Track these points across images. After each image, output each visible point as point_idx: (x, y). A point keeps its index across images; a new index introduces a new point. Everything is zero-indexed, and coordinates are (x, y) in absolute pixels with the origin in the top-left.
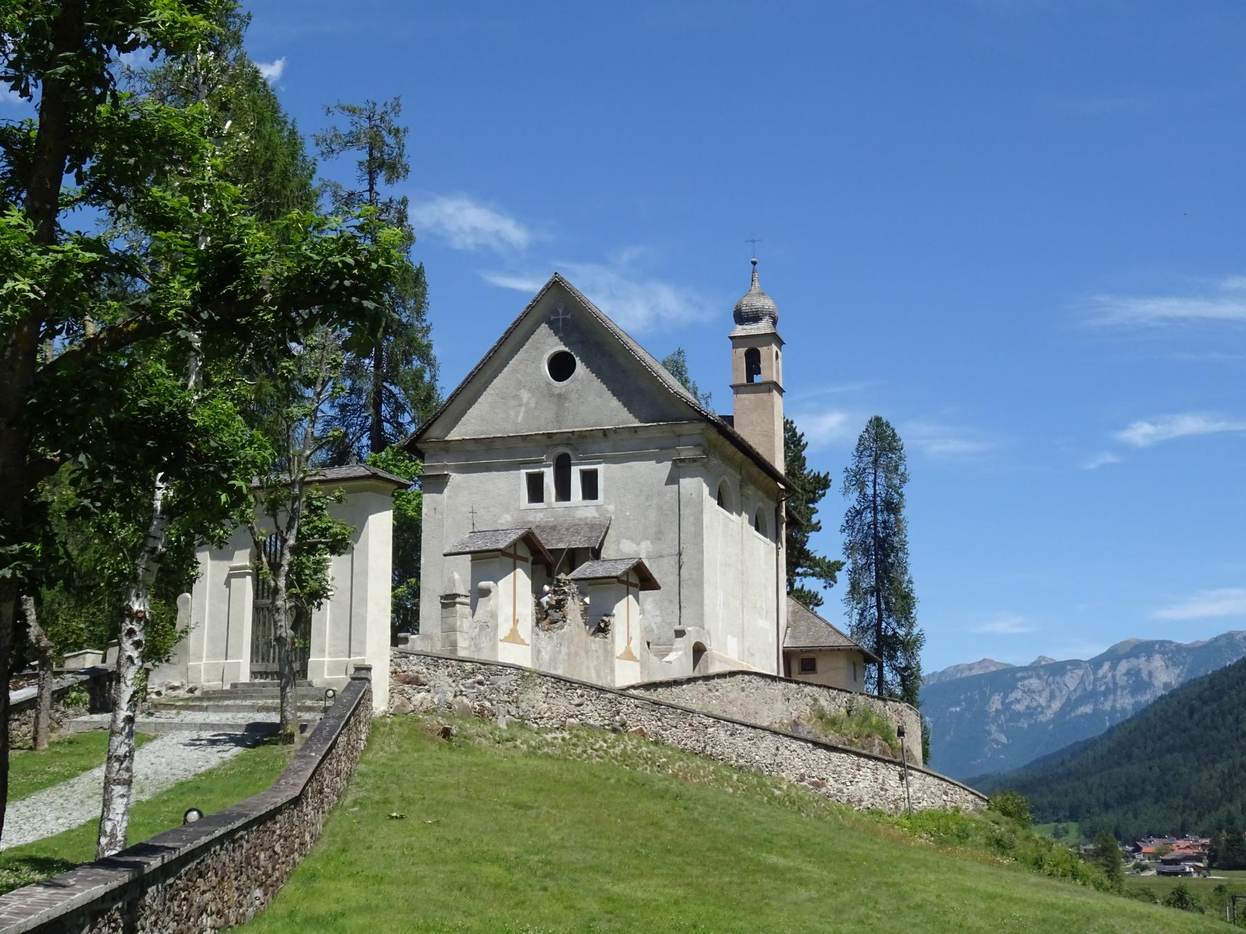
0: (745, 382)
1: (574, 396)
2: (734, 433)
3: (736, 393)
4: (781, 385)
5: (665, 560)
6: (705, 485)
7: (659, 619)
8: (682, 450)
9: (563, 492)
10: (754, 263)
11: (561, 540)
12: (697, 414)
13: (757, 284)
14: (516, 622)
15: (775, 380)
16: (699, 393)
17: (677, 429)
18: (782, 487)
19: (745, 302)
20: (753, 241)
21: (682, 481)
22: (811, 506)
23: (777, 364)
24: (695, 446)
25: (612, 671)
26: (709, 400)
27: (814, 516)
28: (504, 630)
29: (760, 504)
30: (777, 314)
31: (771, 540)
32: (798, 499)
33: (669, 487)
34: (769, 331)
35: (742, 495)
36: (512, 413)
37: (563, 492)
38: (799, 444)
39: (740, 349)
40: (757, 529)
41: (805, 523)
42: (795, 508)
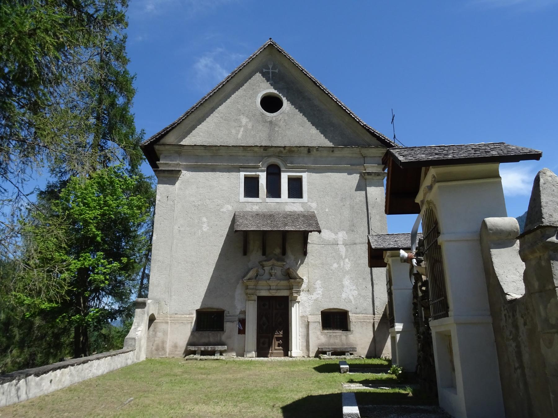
1: (281, 123)
5: (358, 247)
7: (356, 293)
36: (234, 131)
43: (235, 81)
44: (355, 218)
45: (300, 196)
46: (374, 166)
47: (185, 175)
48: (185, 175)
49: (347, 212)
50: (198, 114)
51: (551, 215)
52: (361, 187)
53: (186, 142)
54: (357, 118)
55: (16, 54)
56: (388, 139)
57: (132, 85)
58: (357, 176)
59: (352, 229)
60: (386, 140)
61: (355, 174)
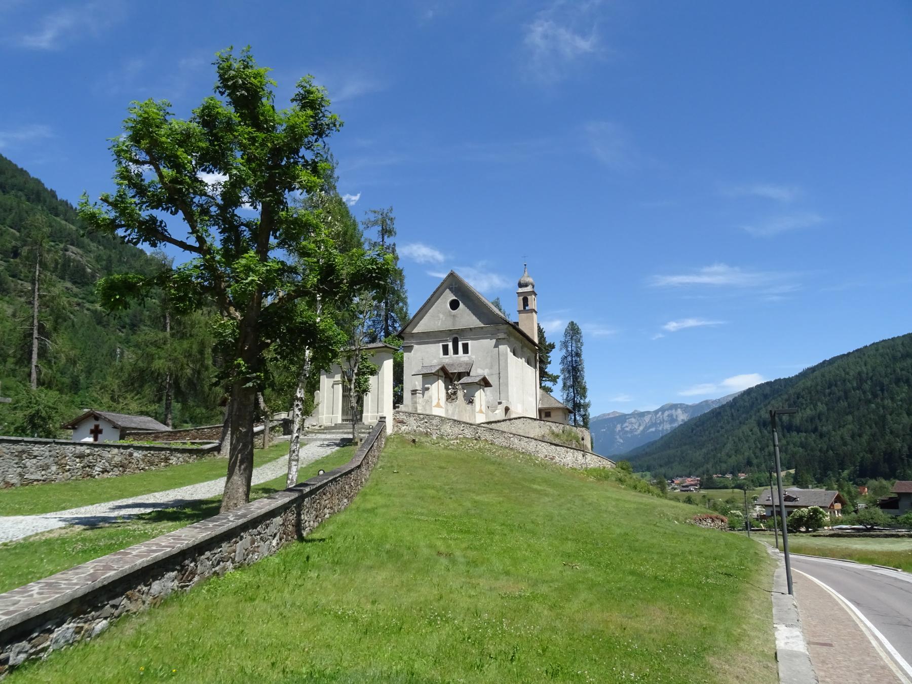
9: (456, 352)
11: (455, 369)
14: (439, 399)
25: (475, 417)
28: (434, 403)
37: (456, 352)
43: (437, 295)
45: (468, 353)
47: (416, 347)
48: (416, 347)
50: (419, 316)
51: (99, 323)
52: (496, 346)
53: (415, 331)
55: (378, 315)
57: (229, 99)
58: (495, 340)
59: (491, 368)
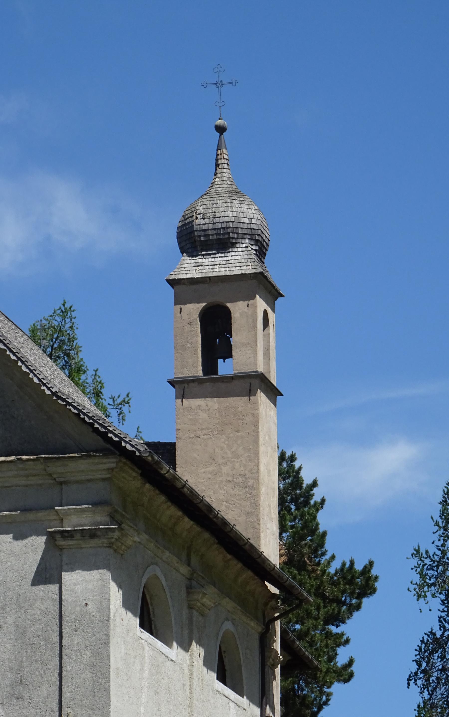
0: (202, 376)
2: (176, 478)
3: (182, 396)
4: (274, 381)
6: (113, 587)
8: (67, 513)
10: (221, 130)
12: (101, 443)
13: (225, 172)
15: (261, 369)
16: (106, 393)
17: (54, 468)
18: (274, 590)
19: (200, 209)
20: (219, 85)
21: (67, 577)
22: (333, 629)
23: (267, 337)
24: (95, 504)
26: (125, 409)
27: (340, 650)
29: (228, 626)
30: (267, 234)
31: (251, 699)
32: (309, 614)
33: (40, 590)
34: (249, 269)
35: (190, 608)
38: (306, 503)
39: (190, 307)
40: (222, 678)
41: (323, 666)
42: (301, 636)
44: (27, 661)
46: (83, 510)
49: (8, 646)
54: (35, 375)
56: (116, 432)
60: (110, 435)
61: (33, 537)
